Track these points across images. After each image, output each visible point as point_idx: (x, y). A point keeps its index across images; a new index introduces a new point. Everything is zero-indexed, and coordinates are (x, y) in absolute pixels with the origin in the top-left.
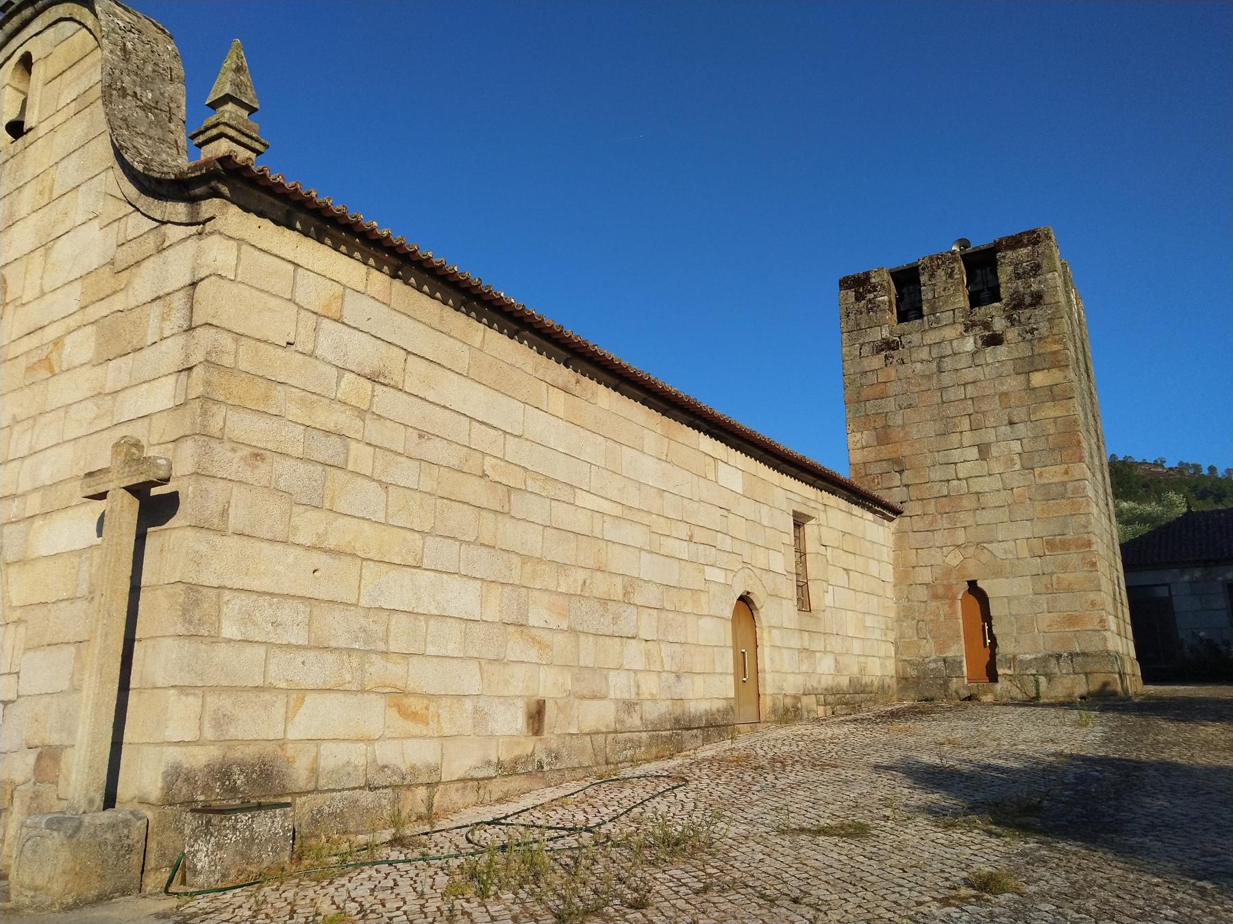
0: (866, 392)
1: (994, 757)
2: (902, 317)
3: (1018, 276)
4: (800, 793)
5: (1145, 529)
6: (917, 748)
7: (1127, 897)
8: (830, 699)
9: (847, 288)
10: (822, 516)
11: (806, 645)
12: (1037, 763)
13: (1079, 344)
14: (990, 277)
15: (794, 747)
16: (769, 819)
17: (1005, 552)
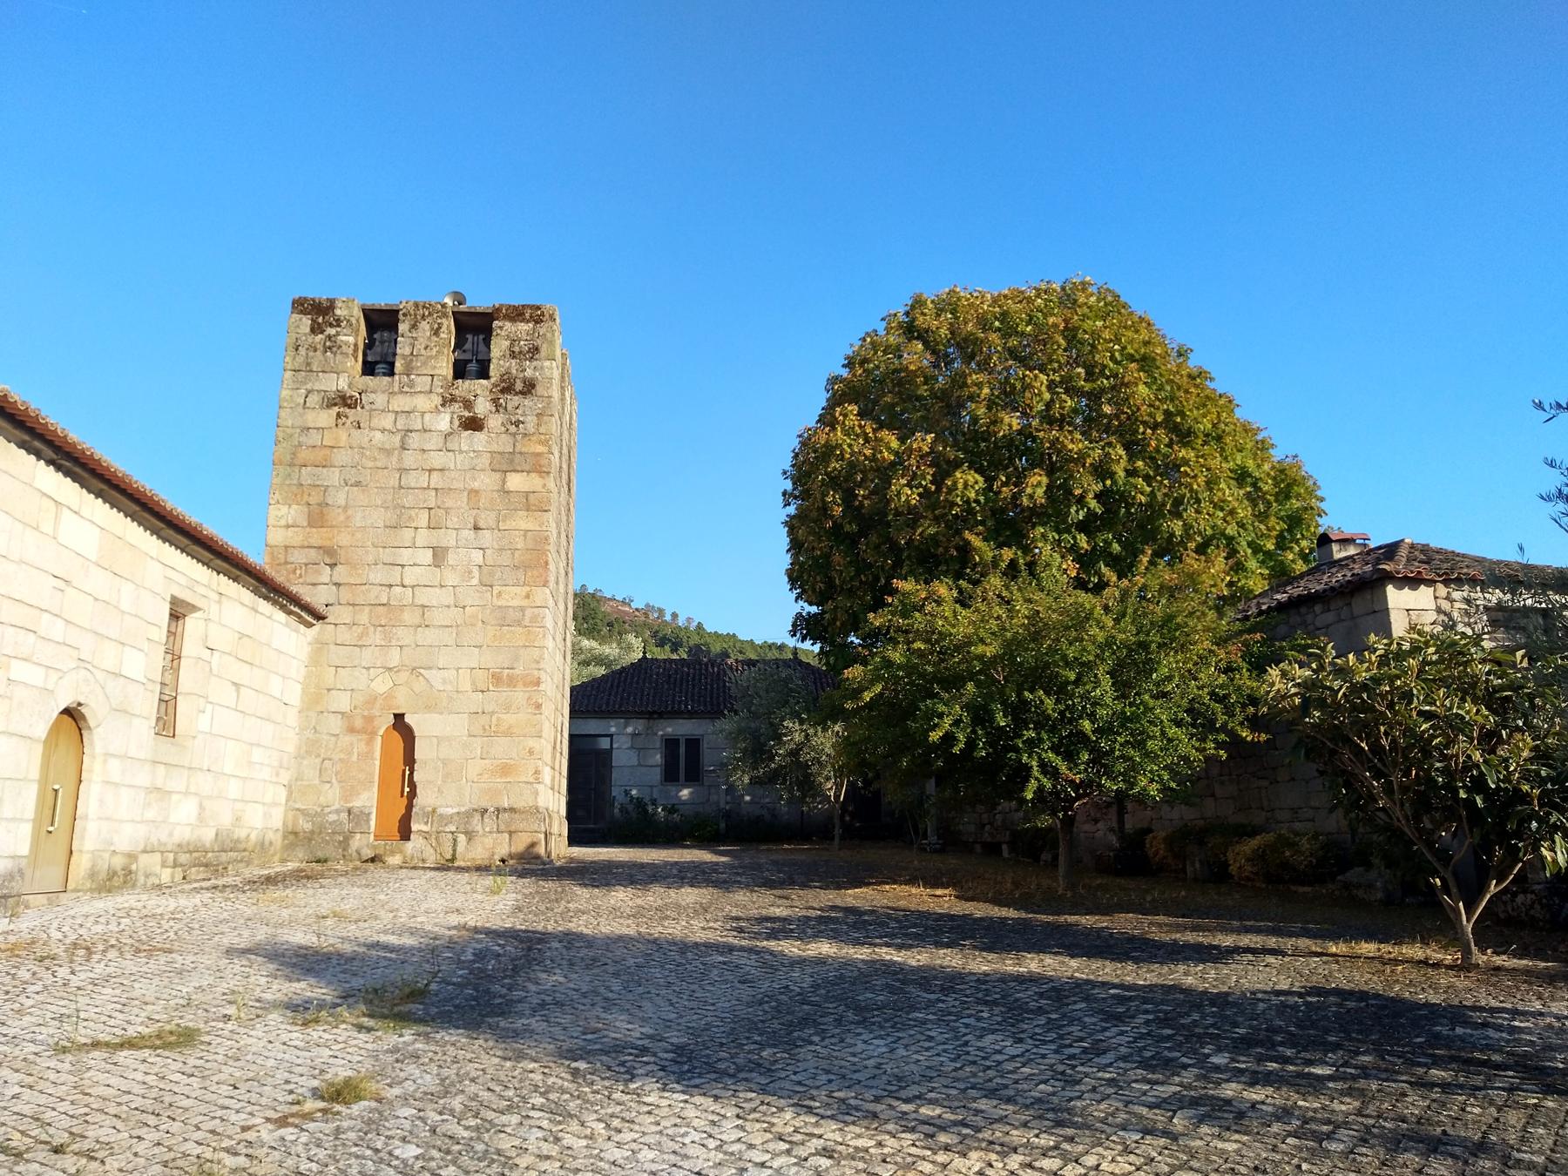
0: (304, 455)
1: (385, 932)
2: (369, 369)
3: (513, 355)
4: (105, 991)
5: (601, 671)
6: (291, 923)
7: (498, 1089)
8: (184, 858)
9: (301, 312)
10: (214, 608)
11: (159, 784)
12: (435, 939)
13: (565, 451)
14: (482, 347)
15: (113, 927)
16: (44, 1034)
17: (444, 682)
